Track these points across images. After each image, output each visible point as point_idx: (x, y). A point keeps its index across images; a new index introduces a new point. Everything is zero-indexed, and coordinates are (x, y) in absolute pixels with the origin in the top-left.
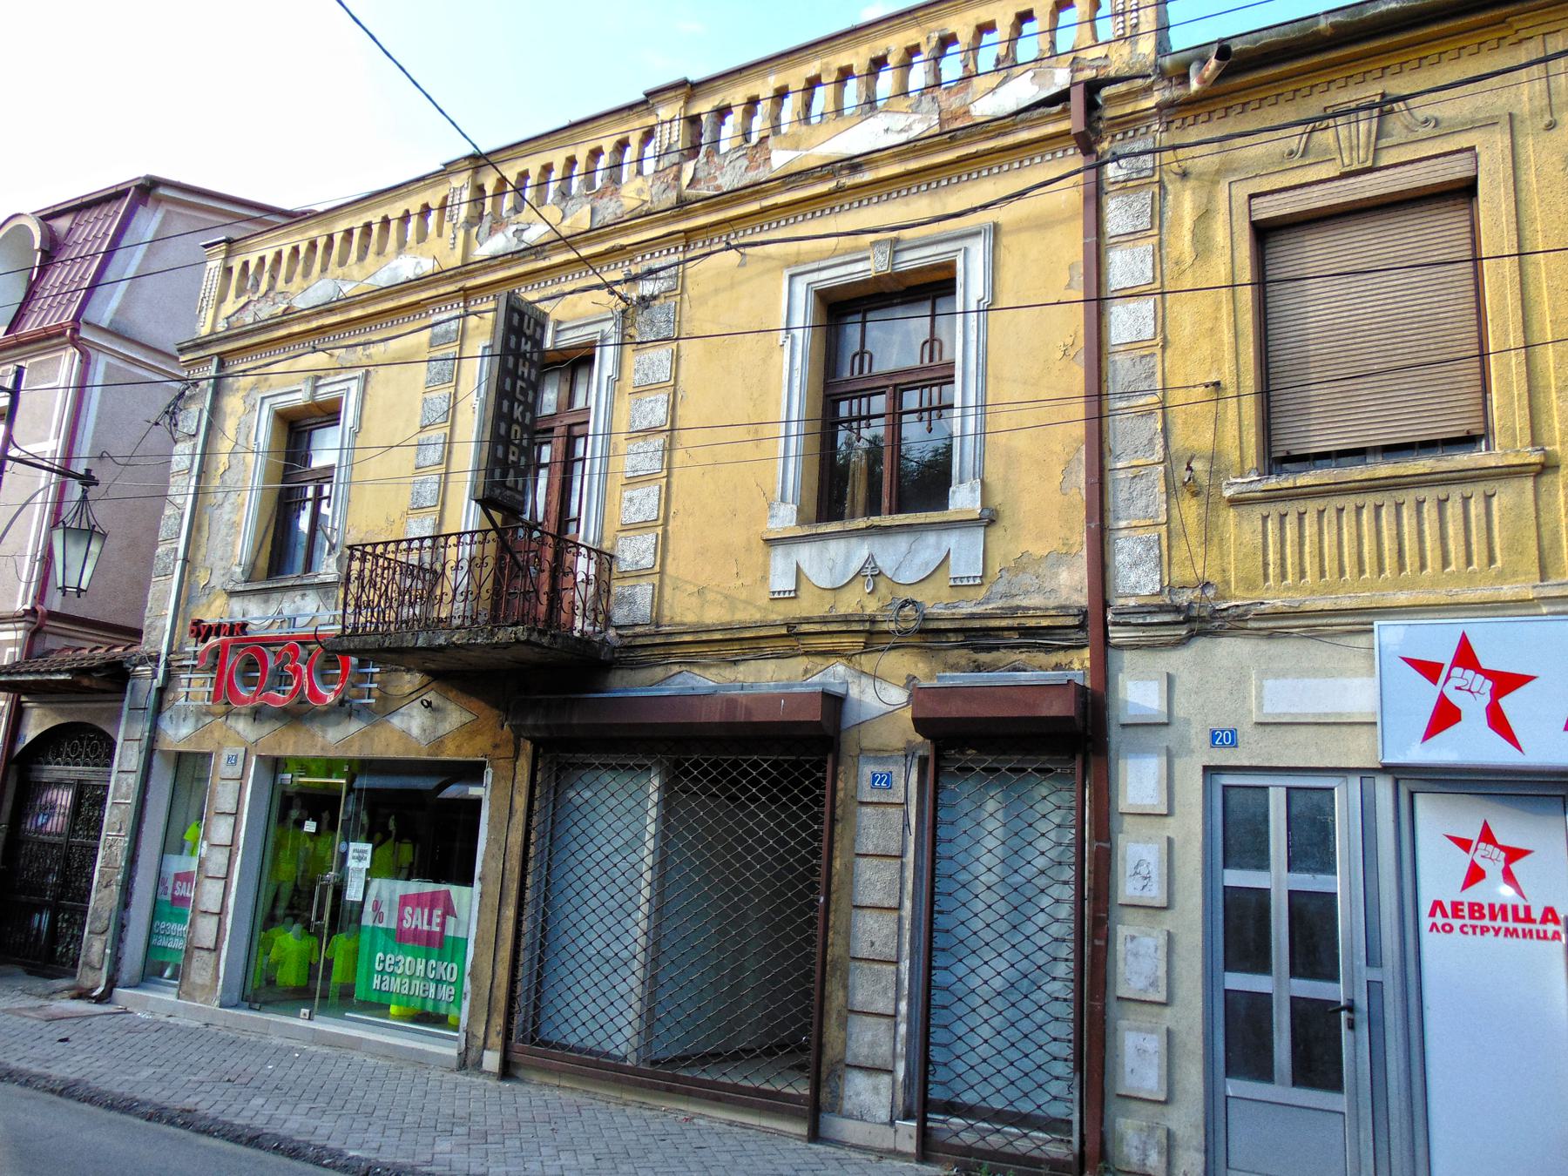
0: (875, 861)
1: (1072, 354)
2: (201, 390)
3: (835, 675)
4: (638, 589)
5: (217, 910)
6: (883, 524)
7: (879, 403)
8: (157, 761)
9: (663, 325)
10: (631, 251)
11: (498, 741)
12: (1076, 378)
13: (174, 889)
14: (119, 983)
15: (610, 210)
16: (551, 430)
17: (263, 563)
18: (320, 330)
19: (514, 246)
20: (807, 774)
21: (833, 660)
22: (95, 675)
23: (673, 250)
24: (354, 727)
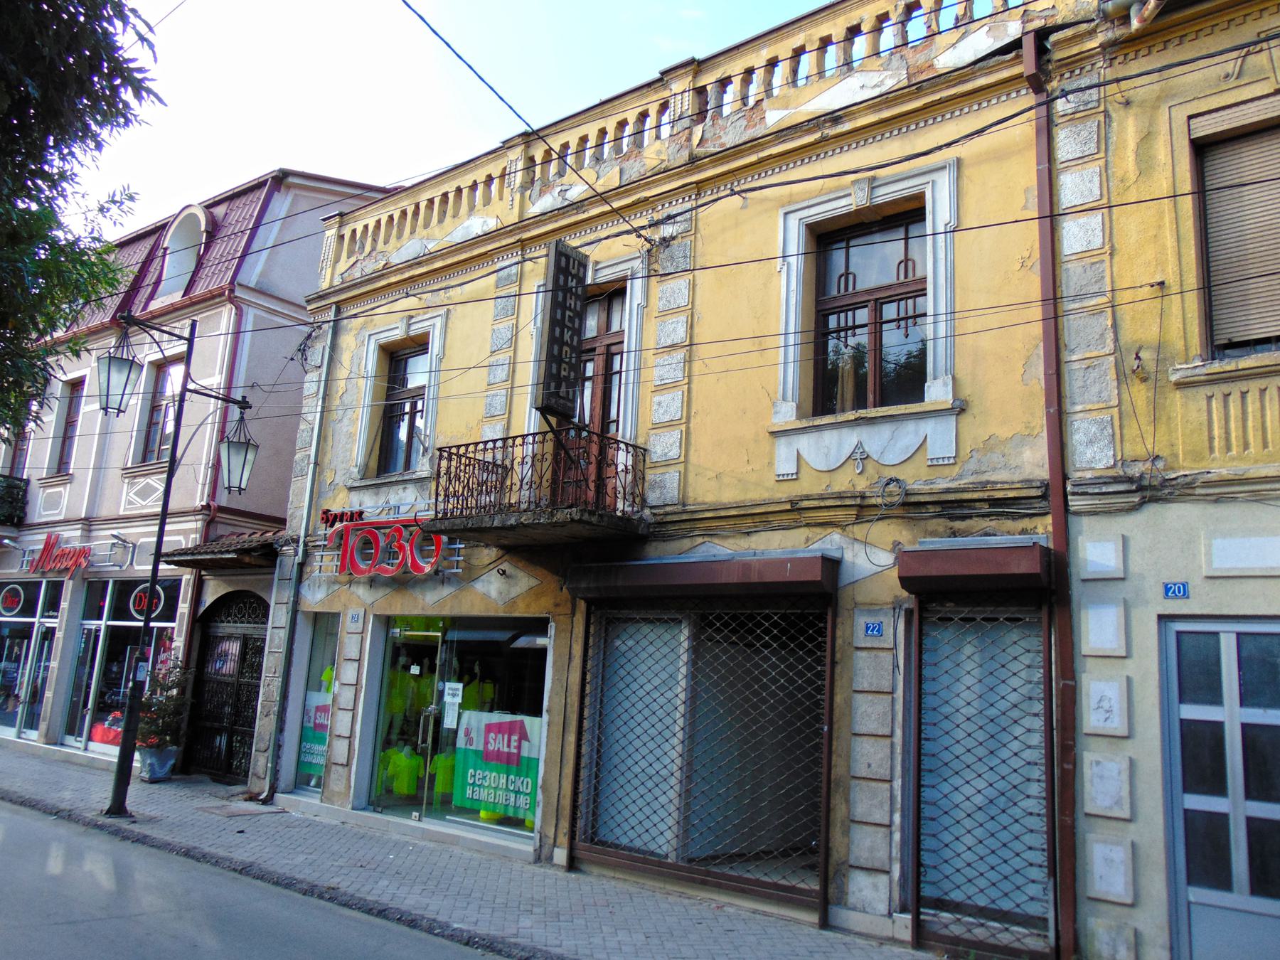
0: (870, 697)
3: (831, 542)
6: (869, 416)
7: (863, 316)
8: (300, 617)
10: (653, 202)
12: (1033, 287)
13: (316, 718)
15: (635, 170)
16: (594, 350)
17: (374, 464)
18: (412, 279)
20: (811, 625)
21: (830, 530)
23: (687, 199)
24: (446, 591)
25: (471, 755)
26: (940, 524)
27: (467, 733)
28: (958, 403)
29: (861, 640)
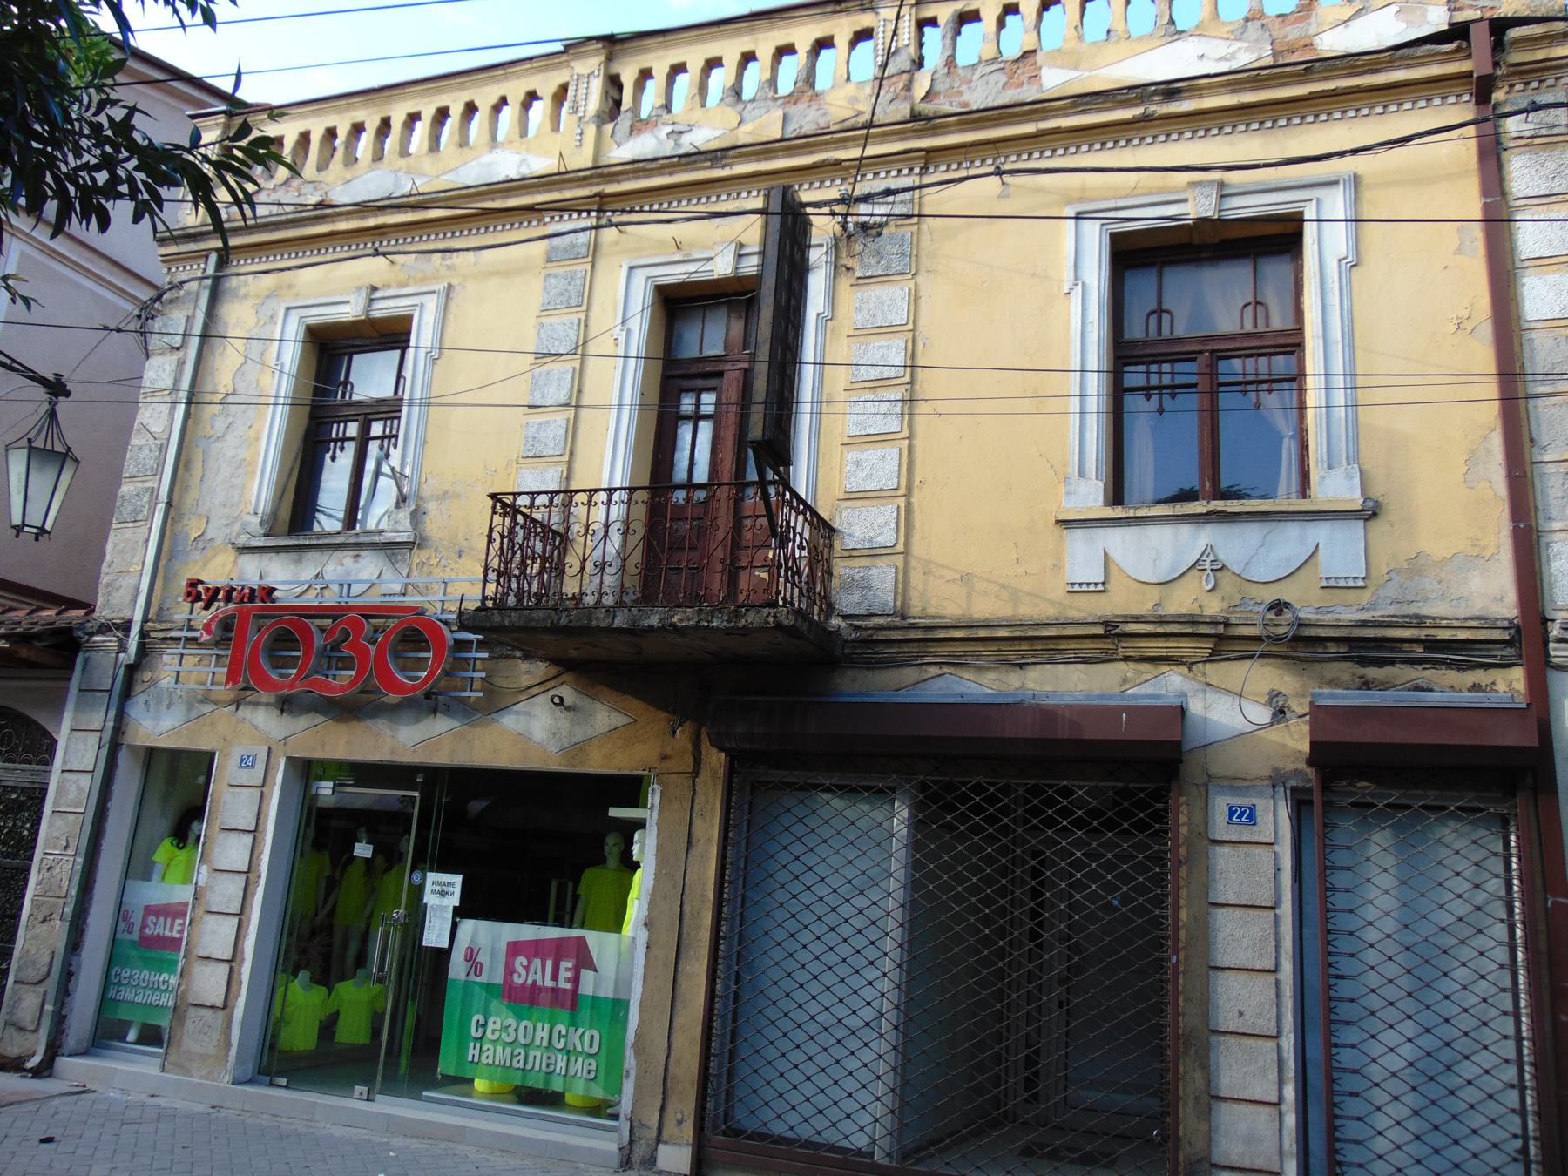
0: (1239, 913)
1: (1469, 328)
2: (188, 293)
3: (1171, 684)
4: (873, 571)
5: (228, 956)
6: (1229, 510)
7: (353, 429)
8: (123, 757)
9: (896, 259)
10: (847, 169)
11: (668, 751)
12: (1484, 357)
13: (144, 927)
14: (65, 1050)
15: (809, 118)
16: (720, 374)
17: (285, 514)
18: (380, 230)
19: (668, 149)
20: (1142, 805)
21: (1164, 668)
22: (37, 644)
23: (905, 171)
24: (441, 725)
25: (479, 996)
26: (1346, 670)
27: (471, 955)
28: (1370, 504)
29: (1221, 828)
